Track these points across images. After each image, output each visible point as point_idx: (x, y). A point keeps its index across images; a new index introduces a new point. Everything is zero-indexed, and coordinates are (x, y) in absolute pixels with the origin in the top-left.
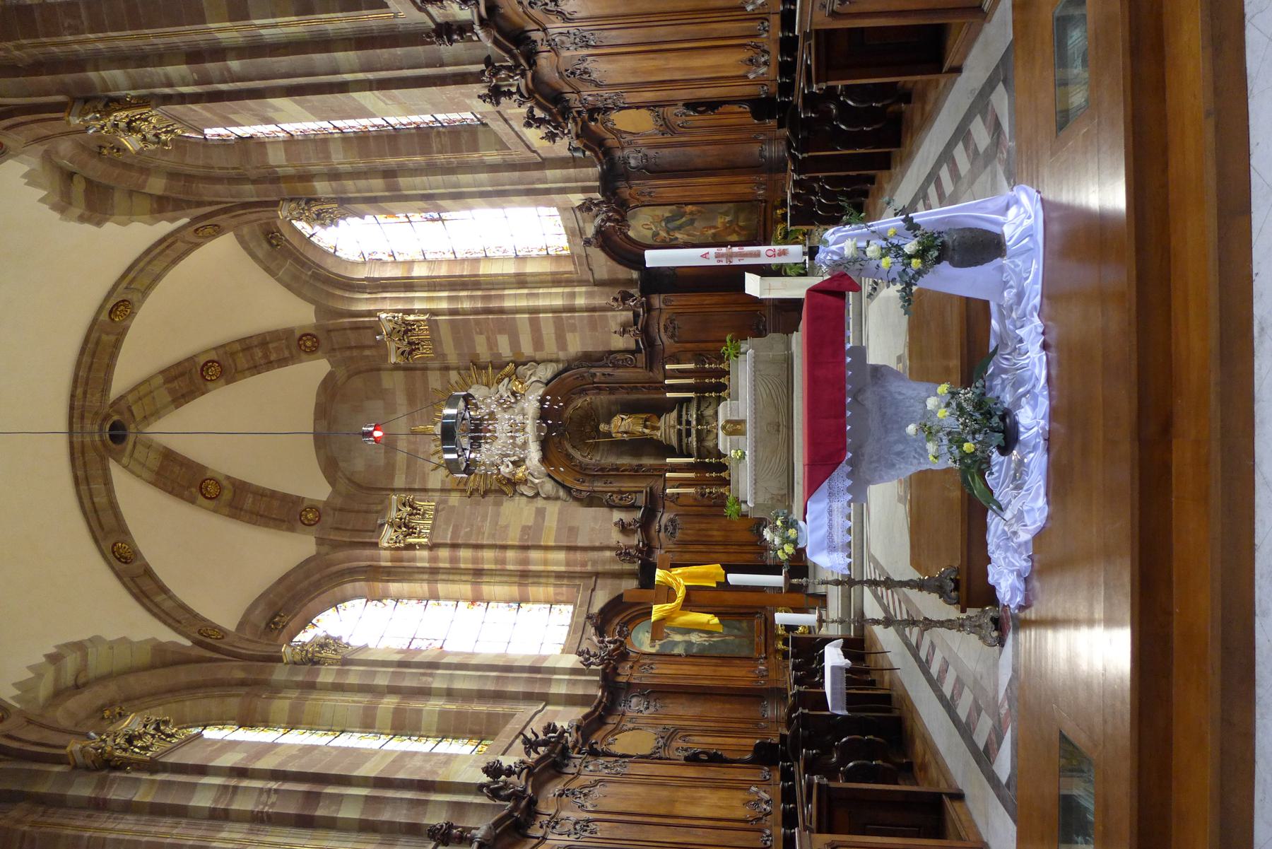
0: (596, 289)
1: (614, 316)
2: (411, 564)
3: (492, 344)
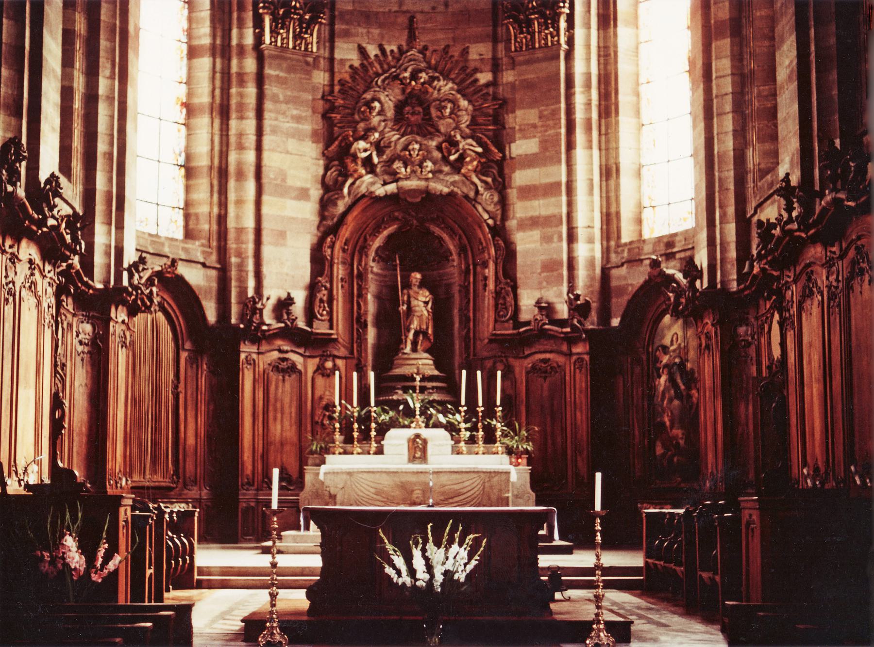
0: (598, 271)
1: (560, 295)
2: (235, 22)
3: (527, 131)
